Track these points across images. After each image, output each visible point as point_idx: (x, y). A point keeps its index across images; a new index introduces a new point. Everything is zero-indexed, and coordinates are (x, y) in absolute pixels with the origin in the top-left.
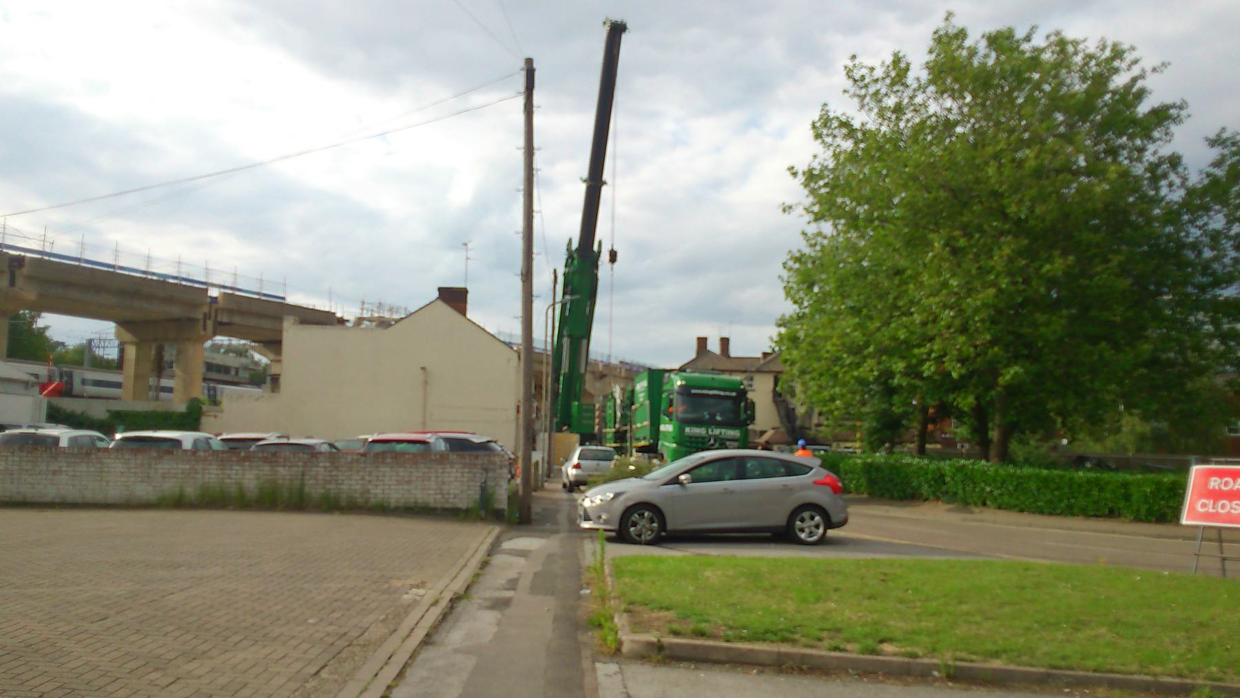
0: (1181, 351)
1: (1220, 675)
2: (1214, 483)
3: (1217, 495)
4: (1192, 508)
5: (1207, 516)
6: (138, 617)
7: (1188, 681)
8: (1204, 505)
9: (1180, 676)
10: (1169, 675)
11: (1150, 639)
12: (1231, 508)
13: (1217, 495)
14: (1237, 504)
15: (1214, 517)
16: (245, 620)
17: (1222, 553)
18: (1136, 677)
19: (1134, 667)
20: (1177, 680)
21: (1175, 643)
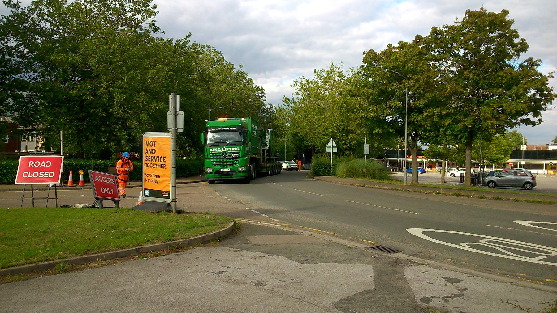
0: (343, 126)
1: (64, 256)
2: (31, 164)
3: (32, 169)
4: (20, 175)
5: (27, 179)
6: (201, 214)
7: (52, 262)
8: (26, 175)
9: (47, 260)
10: (41, 261)
11: (24, 244)
12: (39, 175)
13: (32, 169)
14: (41, 173)
15: (32, 179)
16: (38, 240)
17: (33, 196)
18: (25, 266)
19: (22, 261)
20: (46, 263)
21: (37, 244)
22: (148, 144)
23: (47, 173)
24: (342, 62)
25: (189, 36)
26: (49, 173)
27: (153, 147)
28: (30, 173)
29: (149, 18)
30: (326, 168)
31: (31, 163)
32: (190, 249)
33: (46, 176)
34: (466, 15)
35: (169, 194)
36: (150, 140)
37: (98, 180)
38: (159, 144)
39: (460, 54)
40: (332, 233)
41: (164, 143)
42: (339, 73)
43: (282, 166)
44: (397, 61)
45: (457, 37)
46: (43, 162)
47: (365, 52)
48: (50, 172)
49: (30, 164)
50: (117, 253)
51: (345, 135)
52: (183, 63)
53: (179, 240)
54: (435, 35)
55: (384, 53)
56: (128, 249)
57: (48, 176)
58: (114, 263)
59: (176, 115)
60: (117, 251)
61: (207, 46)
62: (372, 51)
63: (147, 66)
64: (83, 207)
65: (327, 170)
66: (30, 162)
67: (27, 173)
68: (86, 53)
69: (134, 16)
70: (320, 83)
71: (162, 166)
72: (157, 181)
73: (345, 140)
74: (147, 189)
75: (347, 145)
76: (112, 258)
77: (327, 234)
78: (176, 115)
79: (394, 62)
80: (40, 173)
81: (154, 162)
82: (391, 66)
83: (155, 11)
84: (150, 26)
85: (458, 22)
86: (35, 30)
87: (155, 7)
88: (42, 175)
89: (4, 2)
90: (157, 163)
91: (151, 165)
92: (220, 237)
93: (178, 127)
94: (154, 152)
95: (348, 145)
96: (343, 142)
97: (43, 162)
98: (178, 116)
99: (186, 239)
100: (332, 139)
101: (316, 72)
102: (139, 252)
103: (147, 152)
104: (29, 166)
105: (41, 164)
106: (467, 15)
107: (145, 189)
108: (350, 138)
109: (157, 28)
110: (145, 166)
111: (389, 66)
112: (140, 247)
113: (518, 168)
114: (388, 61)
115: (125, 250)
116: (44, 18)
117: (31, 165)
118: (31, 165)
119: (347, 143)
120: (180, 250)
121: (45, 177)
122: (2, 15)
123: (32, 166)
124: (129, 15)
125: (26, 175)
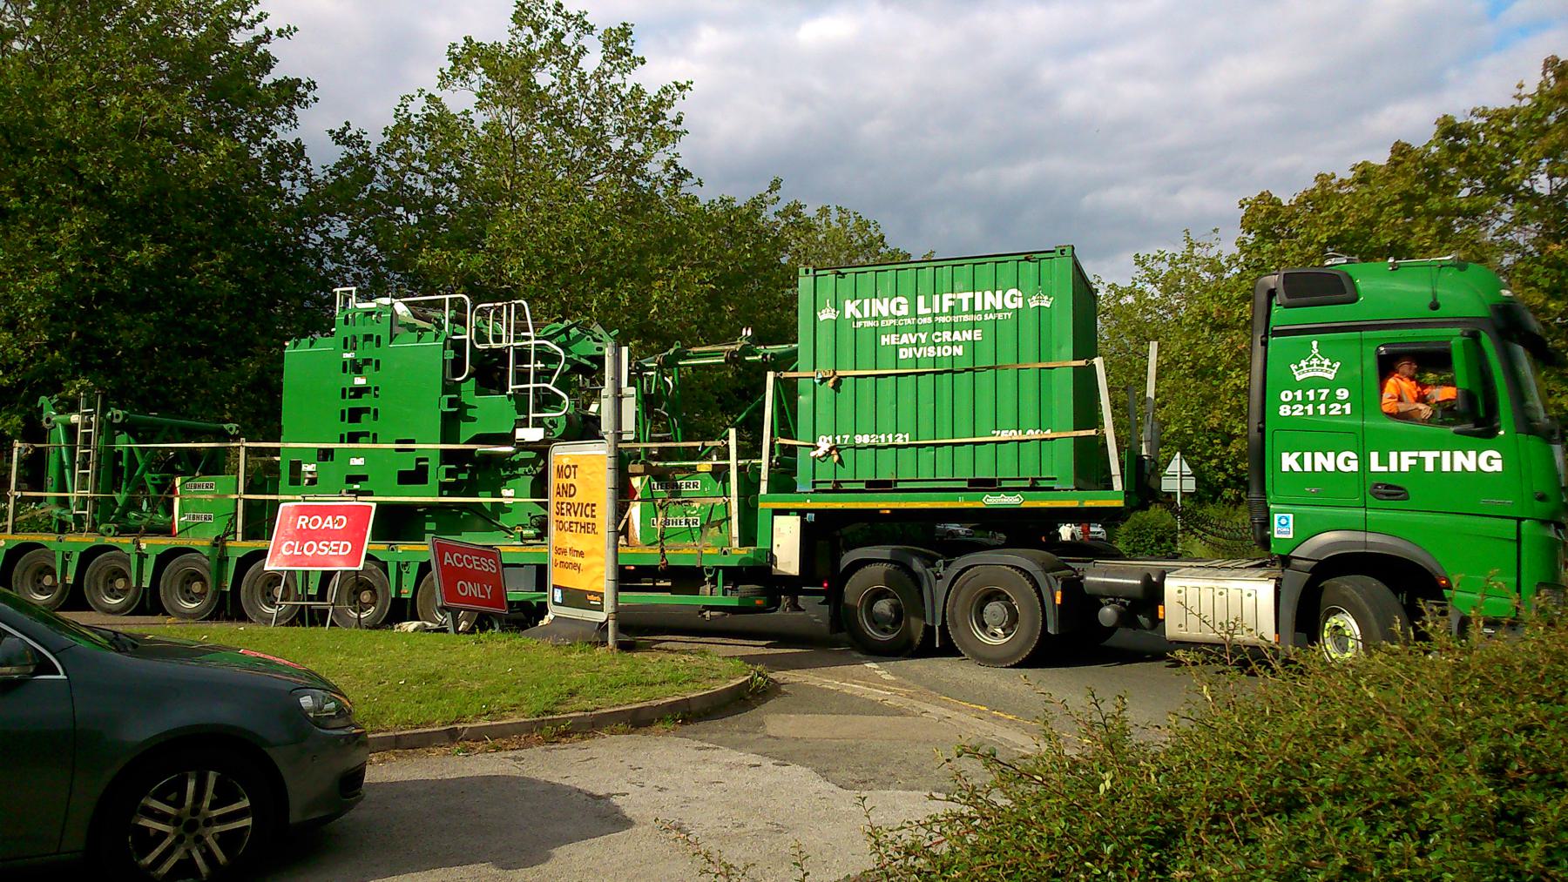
22: (560, 472)
23: (335, 545)
24: (1216, 230)
25: (776, 185)
26: (338, 545)
27: (571, 480)
28: (298, 543)
29: (662, 149)
30: (1161, 540)
31: (303, 520)
32: (593, 737)
33: (334, 551)
34: (1544, 74)
35: (602, 598)
36: (566, 462)
37: (451, 561)
38: (582, 471)
39: (1537, 189)
40: (1010, 717)
41: (594, 469)
42: (1212, 261)
43: (1060, 535)
44: (1341, 223)
45: (1518, 140)
46: (330, 518)
47: (1245, 199)
48: (343, 543)
49: (300, 522)
50: (397, 737)
51: (1218, 441)
52: (748, 260)
53: (574, 710)
54: (1452, 138)
55: (1307, 199)
56: (427, 730)
57: (337, 551)
58: (383, 761)
59: (618, 399)
60: (397, 733)
61: (839, 209)
62: (1265, 197)
63: (655, 272)
64: (415, 630)
65: (1163, 545)
66: (301, 517)
67: (292, 543)
68: (500, 245)
69: (631, 147)
70: (1151, 291)
71: (588, 528)
72: (576, 567)
73: (1218, 457)
74: (559, 587)
75: (1225, 470)
76: (383, 748)
77: (998, 718)
78: (618, 399)
79: (1330, 223)
80: (321, 544)
81: (573, 518)
82: (1323, 238)
83: (679, 128)
84: (667, 170)
85: (1525, 96)
86: (400, 195)
87: (678, 122)
88: (324, 549)
89: (331, 132)
90: (578, 519)
91: (567, 525)
92: (689, 713)
93: (624, 429)
94: (572, 492)
95: (1231, 471)
96: (1214, 462)
97: (330, 518)
98: (624, 400)
99: (586, 711)
100: (1178, 454)
101: (1141, 262)
102: (452, 736)
103: (558, 493)
104: (298, 527)
105: (323, 522)
106: (1549, 74)
107: (555, 587)
108: (1234, 450)
109: (682, 172)
110: (555, 528)
111: (1316, 235)
112: (459, 726)
113: (87, 512)
114: (1316, 225)
115: (420, 730)
116: (413, 164)
117: (301, 526)
118: (301, 526)
119: (1228, 466)
120: (564, 740)
121: (331, 553)
122: (323, 167)
123: (304, 527)
124: (617, 144)
125: (291, 548)
